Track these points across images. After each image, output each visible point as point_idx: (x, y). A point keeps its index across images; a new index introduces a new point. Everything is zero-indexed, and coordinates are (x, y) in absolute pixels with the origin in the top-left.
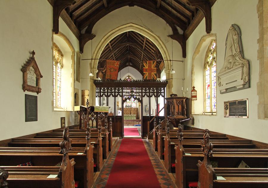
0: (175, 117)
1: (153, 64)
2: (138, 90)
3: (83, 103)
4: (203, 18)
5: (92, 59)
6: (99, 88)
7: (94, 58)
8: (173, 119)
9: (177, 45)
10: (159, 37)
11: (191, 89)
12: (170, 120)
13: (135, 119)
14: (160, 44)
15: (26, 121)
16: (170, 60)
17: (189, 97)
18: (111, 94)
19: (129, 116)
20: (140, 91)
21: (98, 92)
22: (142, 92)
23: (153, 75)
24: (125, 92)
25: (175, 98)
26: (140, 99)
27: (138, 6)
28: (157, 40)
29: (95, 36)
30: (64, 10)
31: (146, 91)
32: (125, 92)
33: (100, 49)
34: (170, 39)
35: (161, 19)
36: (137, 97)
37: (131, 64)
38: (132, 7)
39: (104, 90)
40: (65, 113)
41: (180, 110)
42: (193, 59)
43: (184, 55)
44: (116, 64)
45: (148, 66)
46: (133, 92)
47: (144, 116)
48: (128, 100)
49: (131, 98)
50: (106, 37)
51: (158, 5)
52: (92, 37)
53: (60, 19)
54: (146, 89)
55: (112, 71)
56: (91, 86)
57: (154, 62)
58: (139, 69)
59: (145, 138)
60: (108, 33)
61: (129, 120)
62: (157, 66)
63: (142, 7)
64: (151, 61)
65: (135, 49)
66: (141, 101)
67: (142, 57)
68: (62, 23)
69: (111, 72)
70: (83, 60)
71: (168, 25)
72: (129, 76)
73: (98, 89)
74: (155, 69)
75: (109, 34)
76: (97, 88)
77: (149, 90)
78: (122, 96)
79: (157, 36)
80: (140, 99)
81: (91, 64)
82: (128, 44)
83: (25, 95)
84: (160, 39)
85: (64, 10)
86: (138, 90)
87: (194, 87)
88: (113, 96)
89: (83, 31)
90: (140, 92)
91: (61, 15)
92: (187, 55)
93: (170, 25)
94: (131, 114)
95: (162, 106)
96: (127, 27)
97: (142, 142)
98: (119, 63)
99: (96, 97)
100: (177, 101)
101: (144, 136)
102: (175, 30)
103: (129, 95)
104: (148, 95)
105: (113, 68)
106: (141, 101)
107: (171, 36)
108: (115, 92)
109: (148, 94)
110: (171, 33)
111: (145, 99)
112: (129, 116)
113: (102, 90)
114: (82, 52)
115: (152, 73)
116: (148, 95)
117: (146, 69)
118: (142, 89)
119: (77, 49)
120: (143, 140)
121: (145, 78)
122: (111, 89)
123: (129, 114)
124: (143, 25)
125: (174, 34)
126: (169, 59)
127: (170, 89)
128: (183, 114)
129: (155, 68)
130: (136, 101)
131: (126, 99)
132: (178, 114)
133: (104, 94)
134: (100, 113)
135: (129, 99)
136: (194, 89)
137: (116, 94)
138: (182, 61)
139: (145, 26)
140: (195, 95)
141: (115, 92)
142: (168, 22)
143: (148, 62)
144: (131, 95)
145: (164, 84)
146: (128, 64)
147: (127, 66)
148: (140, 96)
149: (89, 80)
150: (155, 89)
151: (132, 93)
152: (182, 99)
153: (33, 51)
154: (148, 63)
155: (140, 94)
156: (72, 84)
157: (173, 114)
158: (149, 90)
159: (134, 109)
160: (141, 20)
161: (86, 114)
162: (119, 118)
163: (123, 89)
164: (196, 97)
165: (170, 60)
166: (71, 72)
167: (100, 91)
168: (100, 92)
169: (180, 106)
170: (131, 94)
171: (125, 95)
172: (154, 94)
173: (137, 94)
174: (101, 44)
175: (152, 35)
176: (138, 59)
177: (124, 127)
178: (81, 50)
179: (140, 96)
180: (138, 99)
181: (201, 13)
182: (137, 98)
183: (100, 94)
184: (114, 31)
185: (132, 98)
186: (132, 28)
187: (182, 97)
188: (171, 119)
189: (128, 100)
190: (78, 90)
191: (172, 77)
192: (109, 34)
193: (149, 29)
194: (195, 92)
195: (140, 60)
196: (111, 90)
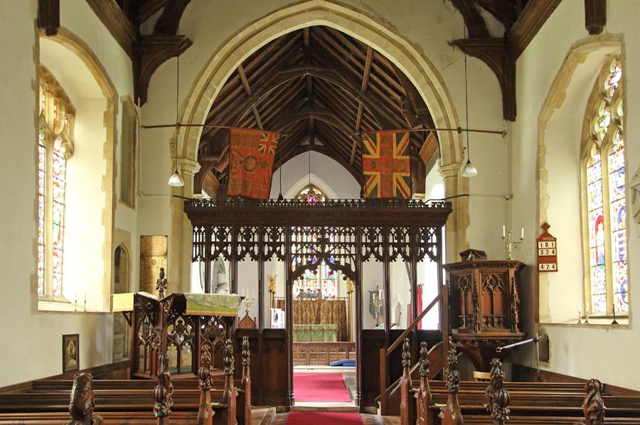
1: (376, 187)
2: (345, 235)
5: (179, 125)
6: (203, 229)
7: (183, 129)
9: (482, 74)
13: (335, 341)
14: (422, 71)
16: (459, 130)
17: (530, 260)
19: (311, 330)
20: (353, 241)
21: (199, 243)
22: (358, 245)
23: (397, 181)
24: (296, 244)
25: (478, 265)
26: (353, 269)
28: (412, 58)
29: (190, 43)
31: (372, 238)
33: (209, 91)
34: (458, 54)
36: (339, 262)
37: (318, 143)
39: (222, 235)
40: (78, 318)
43: (510, 111)
44: (264, 143)
45: (378, 151)
48: (308, 273)
49: (319, 263)
50: (228, 47)
52: (178, 46)
54: (371, 232)
59: (372, 408)
64: (389, 133)
65: (331, 102)
67: (359, 117)
70: (146, 127)
72: (311, 186)
73: (199, 231)
75: (241, 36)
76: (196, 229)
78: (286, 258)
79: (410, 43)
80: (353, 269)
81: (174, 143)
82: (309, 71)
84: (423, 56)
87: (546, 226)
89: (148, 27)
90: (350, 244)
94: (318, 321)
95: (430, 292)
96: (303, 12)
98: (274, 141)
99: (194, 260)
101: (368, 394)
102: (474, 22)
103: (312, 255)
104: (381, 254)
106: (354, 276)
107: (462, 45)
109: (381, 249)
110: (461, 31)
111: (372, 269)
112: (311, 330)
113: (213, 237)
114: (144, 101)
116: (381, 254)
117: (373, 161)
118: (358, 234)
119: (125, 88)
121: (369, 191)
124: (362, 4)
126: (454, 126)
127: (460, 232)
128: (507, 324)
129: (404, 157)
130: (338, 275)
131: (301, 270)
132: (490, 321)
133: (221, 250)
135: (313, 267)
137: (266, 249)
138: (503, 133)
139: (371, 9)
140: (550, 253)
143: (378, 135)
144: (318, 254)
146: (307, 143)
147: (305, 149)
148: (351, 256)
149: (169, 198)
151: (323, 248)
152: (503, 270)
155: (353, 252)
156: (104, 214)
157: (471, 322)
158: (385, 234)
159: (332, 303)
161: (155, 323)
165: (459, 130)
166: (104, 173)
167: (209, 238)
168: (208, 243)
169: (497, 295)
171: (296, 255)
172: (376, 249)
173: (343, 251)
175: (393, 41)
177: (295, 371)
179: (351, 256)
180: (346, 269)
182: (343, 263)
183: (208, 251)
184: (257, 26)
188: (464, 342)
189: (307, 271)
192: (241, 36)
193: (381, 20)
194: (550, 244)
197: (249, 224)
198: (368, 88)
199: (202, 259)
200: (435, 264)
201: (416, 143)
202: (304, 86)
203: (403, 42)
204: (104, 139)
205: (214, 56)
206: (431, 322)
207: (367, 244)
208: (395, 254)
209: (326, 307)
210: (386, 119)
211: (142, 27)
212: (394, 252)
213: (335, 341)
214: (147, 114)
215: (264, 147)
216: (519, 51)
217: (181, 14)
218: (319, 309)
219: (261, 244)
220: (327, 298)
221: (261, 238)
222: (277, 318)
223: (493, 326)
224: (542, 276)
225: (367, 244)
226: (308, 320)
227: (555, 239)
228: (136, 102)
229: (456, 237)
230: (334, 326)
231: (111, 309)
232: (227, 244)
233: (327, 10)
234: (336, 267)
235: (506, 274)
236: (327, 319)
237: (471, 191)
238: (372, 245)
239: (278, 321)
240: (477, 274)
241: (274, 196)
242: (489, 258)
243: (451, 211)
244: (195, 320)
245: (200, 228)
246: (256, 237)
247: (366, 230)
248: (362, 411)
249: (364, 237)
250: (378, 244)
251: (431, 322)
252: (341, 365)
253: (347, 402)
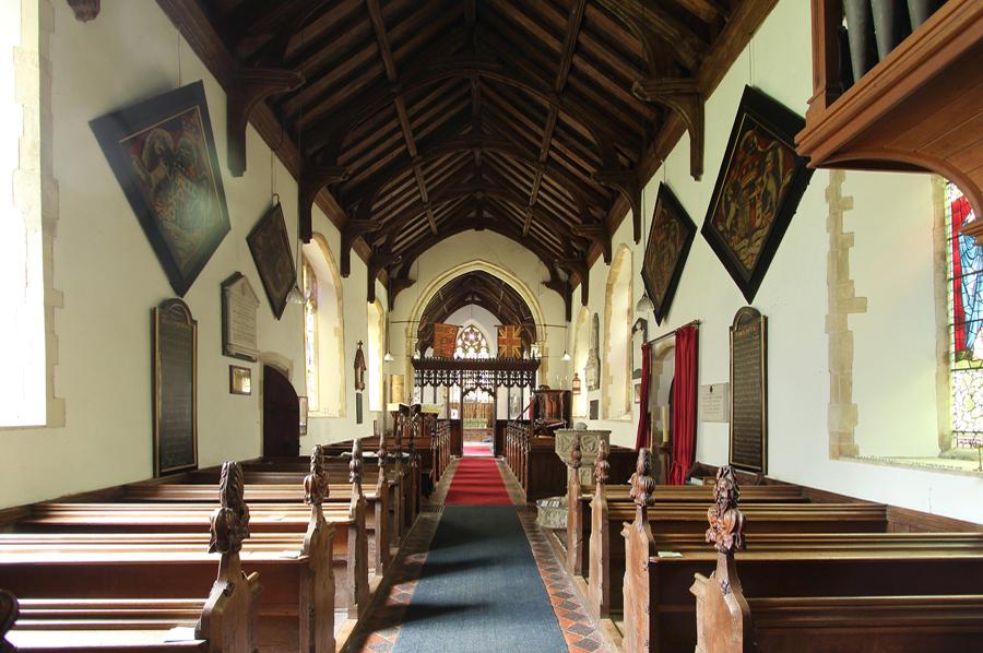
3: (403, 400)
9: (555, 298)
22: (496, 379)
29: (415, 282)
37: (477, 299)
39: (429, 374)
42: (577, 329)
43: (569, 317)
51: (543, 157)
52: (409, 283)
62: (523, 335)
66: (494, 395)
72: (472, 326)
77: (509, 374)
78: (461, 386)
81: (407, 330)
88: (432, 385)
89: (395, 273)
94: (475, 416)
95: (527, 402)
102: (554, 273)
106: (494, 395)
107: (548, 285)
108: (448, 379)
111: (502, 391)
118: (496, 374)
119: (386, 308)
125: (371, 595)
130: (486, 393)
131: (467, 391)
132: (550, 415)
135: (473, 390)
136: (576, 379)
141: (448, 379)
146: (470, 299)
147: (469, 303)
157: (543, 417)
158: (509, 374)
159: (484, 405)
161: (407, 416)
164: (578, 389)
178: (391, 306)
180: (490, 391)
193: (509, 271)
198: (568, 86)
200: (459, 389)
202: (462, 106)
206: (526, 416)
211: (392, 273)
230: (486, 420)
234: (484, 390)
235: (558, 396)
238: (502, 379)
239: (455, 415)
240: (546, 396)
241: (455, 357)
251: (526, 416)
253: (491, 454)
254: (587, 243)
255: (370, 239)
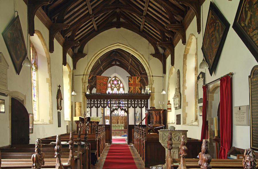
0: (154, 125)
1: (132, 90)
2: (125, 101)
3: (81, 114)
4: (179, 40)
5: (84, 75)
6: (89, 100)
7: (85, 76)
8: (152, 127)
10: (142, 55)
11: (167, 102)
12: (150, 128)
13: (123, 129)
14: (144, 61)
15: (58, 127)
16: (152, 76)
17: (167, 109)
18: (101, 105)
19: (115, 126)
20: (127, 103)
21: (89, 104)
22: (128, 104)
23: (137, 89)
25: (154, 110)
26: (127, 110)
27: (124, 27)
28: (141, 58)
30: (40, 8)
31: (131, 102)
32: (113, 104)
33: (91, 66)
34: (152, 57)
35: (144, 39)
37: (118, 63)
38: (119, 29)
39: (94, 102)
40: (67, 122)
41: (158, 120)
42: (169, 78)
43: (164, 72)
45: (133, 81)
46: (120, 103)
47: (129, 124)
49: (118, 108)
50: (96, 55)
52: (84, 55)
53: (36, 18)
54: (131, 101)
55: (101, 86)
56: (83, 99)
57: (138, 77)
58: (128, 69)
59: (131, 144)
60: (98, 52)
61: (116, 130)
62: (141, 81)
63: (127, 29)
64: (135, 77)
66: (127, 112)
68: (37, 21)
69: (101, 86)
70: (76, 75)
71: (150, 44)
72: (115, 77)
73: (89, 100)
74: (139, 84)
75: (99, 52)
76: (88, 100)
78: (110, 107)
79: (141, 54)
80: (127, 110)
83: (58, 112)
84: (144, 57)
85: (40, 8)
86: (125, 101)
87: (169, 101)
89: (76, 50)
90: (126, 104)
91: (36, 14)
92: (219, 9)
93: (152, 45)
94: (118, 123)
96: (114, 46)
97: (128, 146)
99: (87, 108)
100: (155, 112)
101: (129, 142)
102: (156, 49)
103: (116, 107)
104: (133, 106)
105: (103, 83)
106: (127, 112)
107: (154, 55)
110: (153, 52)
111: (131, 110)
112: (115, 126)
113: (92, 102)
114: (75, 69)
115: (137, 87)
116: (133, 106)
118: (128, 101)
119: (72, 68)
120: (129, 145)
121: (130, 91)
122: (101, 100)
123: (116, 123)
124: (129, 45)
126: (151, 75)
127: (152, 101)
128: (160, 123)
129: (139, 83)
132: (156, 122)
133: (94, 105)
134: (94, 122)
135: (117, 109)
138: (163, 77)
139: (131, 46)
140: (170, 107)
142: (150, 42)
143: (133, 77)
144: (118, 106)
145: (147, 97)
146: (114, 63)
147: (113, 65)
148: (126, 107)
149: (82, 93)
150: (139, 100)
151: (119, 105)
152: (159, 111)
153: (60, 85)
154: (133, 79)
155: (127, 106)
156: (69, 98)
157: (152, 123)
158: (134, 101)
159: (122, 117)
160: (127, 41)
161: (83, 123)
162: (107, 126)
163: (111, 101)
164: (170, 109)
165: (152, 76)
166: (69, 89)
167: (91, 102)
168: (91, 104)
169: (158, 117)
170: (118, 105)
173: (124, 106)
174: (91, 61)
175: (137, 53)
176: (127, 62)
177: (112, 138)
178: (75, 67)
179: (126, 107)
180: (125, 110)
181: (179, 35)
182: (124, 108)
183: (91, 106)
184: (103, 50)
185: (119, 108)
186: (118, 46)
187: (160, 109)
188: (151, 127)
189: (115, 110)
190: (73, 102)
191: (154, 91)
192: (99, 52)
193: (134, 49)
194: (170, 105)
195: (128, 63)
196: (101, 102)
197: (101, 99)
199: (90, 108)
201: (178, 18)
203: (139, 54)
204: (69, 81)
205: (92, 58)
207: (130, 104)
208: (137, 106)
209: (120, 119)
210: (138, 64)
212: (137, 106)
213: (123, 129)
214: (77, 72)
215: (105, 80)
216: (166, 58)
217: (84, 47)
218: (118, 119)
219: (104, 104)
220: (121, 115)
221: (104, 102)
222: (107, 122)
223: (157, 123)
224: (168, 112)
225: (130, 104)
226: (114, 123)
227: (171, 104)
228: (74, 70)
229: (152, 102)
230: (123, 125)
231: (135, 123)
232: (95, 104)
233: (120, 45)
234: (122, 109)
236: (121, 123)
237: (155, 91)
239: (107, 122)
241: (107, 93)
242: (156, 109)
243: (150, 96)
244: (91, 122)
245: (89, 100)
246: (103, 102)
247: (130, 100)
248: (129, 144)
249: (129, 102)
250: (133, 104)
251: (144, 123)
252: (125, 136)
254: (173, 34)
255: (63, 33)
